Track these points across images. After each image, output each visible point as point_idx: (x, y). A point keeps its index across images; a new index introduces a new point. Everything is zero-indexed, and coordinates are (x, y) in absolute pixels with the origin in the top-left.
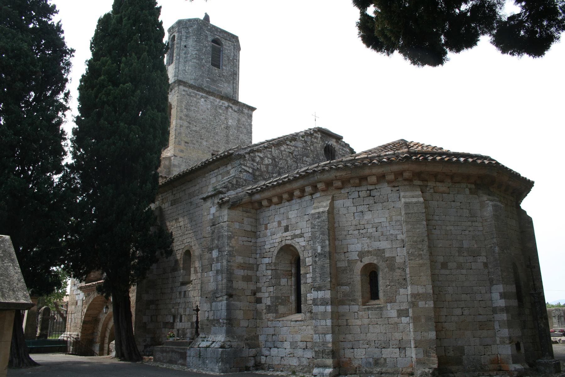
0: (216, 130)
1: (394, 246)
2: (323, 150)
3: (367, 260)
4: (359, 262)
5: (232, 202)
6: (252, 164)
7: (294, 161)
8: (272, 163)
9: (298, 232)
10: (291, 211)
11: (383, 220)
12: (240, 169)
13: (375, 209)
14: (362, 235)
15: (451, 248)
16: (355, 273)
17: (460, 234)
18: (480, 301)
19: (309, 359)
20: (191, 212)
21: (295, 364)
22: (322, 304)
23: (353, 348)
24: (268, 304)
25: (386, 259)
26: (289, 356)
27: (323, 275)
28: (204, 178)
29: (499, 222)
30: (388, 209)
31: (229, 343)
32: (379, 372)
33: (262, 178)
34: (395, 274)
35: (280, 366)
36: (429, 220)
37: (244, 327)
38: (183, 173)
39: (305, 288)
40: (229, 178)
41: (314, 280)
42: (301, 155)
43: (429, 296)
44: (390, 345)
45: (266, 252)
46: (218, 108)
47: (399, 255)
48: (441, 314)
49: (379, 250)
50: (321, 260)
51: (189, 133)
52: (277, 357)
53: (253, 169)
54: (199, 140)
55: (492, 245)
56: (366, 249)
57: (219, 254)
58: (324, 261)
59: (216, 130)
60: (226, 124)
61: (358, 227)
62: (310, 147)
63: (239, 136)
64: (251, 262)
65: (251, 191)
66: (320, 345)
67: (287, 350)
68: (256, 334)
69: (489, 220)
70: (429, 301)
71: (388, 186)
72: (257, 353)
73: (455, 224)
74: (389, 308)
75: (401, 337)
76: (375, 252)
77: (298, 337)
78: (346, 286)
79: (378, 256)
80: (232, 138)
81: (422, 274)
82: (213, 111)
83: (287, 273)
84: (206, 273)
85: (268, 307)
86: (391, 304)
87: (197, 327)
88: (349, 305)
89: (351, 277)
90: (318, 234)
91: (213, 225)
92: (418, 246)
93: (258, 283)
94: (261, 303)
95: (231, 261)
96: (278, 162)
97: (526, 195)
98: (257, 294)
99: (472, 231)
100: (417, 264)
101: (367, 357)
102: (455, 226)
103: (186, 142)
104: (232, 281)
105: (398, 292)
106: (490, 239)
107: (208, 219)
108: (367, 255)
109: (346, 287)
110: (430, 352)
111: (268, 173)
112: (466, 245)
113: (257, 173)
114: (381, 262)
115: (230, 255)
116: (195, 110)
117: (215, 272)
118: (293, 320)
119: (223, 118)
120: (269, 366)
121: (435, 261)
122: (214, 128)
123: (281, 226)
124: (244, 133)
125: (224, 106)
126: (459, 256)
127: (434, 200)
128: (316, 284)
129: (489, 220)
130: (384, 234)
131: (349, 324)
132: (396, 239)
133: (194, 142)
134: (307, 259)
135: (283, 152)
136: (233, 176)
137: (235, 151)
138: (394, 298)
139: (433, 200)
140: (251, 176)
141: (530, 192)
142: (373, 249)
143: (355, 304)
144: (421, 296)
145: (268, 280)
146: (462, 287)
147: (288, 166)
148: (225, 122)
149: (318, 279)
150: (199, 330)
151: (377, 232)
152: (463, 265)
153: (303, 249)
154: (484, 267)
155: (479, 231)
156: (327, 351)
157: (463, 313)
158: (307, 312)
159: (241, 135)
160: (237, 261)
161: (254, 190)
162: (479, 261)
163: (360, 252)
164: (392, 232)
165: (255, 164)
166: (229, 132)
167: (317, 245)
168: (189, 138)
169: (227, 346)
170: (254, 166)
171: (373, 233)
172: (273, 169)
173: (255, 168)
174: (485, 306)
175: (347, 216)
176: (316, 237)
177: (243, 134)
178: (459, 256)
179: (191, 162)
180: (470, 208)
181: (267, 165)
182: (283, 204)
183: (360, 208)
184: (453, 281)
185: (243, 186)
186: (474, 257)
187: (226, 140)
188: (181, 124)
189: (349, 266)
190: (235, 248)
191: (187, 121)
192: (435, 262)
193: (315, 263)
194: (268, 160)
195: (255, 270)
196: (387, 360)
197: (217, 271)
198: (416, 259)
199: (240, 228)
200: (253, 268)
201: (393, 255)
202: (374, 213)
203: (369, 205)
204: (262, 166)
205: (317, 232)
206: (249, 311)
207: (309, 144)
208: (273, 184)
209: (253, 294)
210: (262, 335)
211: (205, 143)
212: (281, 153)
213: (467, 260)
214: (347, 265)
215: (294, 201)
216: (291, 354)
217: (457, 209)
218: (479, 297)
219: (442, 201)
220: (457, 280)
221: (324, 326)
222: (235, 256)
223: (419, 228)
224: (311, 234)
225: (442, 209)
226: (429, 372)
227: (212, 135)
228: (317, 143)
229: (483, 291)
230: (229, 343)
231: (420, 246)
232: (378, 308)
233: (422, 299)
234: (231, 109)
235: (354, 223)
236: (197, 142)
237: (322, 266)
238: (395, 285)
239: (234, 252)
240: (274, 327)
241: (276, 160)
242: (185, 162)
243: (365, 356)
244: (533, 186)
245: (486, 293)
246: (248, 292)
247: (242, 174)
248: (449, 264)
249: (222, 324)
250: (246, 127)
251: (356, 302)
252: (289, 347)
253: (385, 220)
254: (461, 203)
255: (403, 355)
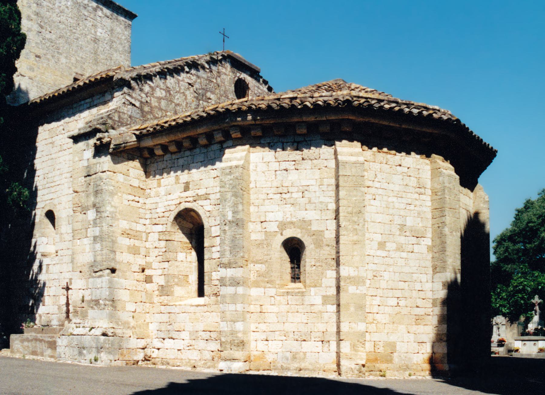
0: (80, 43)
1: (323, 218)
2: (233, 85)
3: (289, 233)
4: (279, 235)
5: (115, 145)
6: (139, 95)
7: (195, 97)
8: (166, 96)
9: (201, 192)
10: (193, 163)
11: (313, 182)
12: (123, 101)
13: (302, 167)
14: (285, 201)
15: (391, 224)
16: (273, 249)
17: (404, 208)
18: (419, 291)
19: (213, 352)
20: (53, 156)
21: (195, 358)
22: (231, 285)
23: (268, 339)
24: (160, 284)
25: (312, 233)
26: (188, 348)
27: (234, 249)
28: (71, 110)
29: (451, 196)
30: (319, 169)
31: (112, 330)
32: (297, 368)
33: (152, 116)
34: (322, 252)
35: (176, 360)
36: (368, 187)
37: (130, 311)
38: (41, 100)
39: (209, 264)
40: (108, 112)
41: (222, 254)
42: (203, 89)
43: (361, 280)
44: (312, 337)
45: (159, 217)
46: (82, 7)
47: (329, 229)
48: (373, 304)
49: (305, 221)
50: (232, 229)
51: (41, 42)
52: (173, 350)
53: (141, 102)
54: (56, 54)
55: (440, 225)
56: (288, 220)
57: (97, 215)
58: (235, 230)
59: (80, 43)
60: (93, 34)
61: (280, 190)
62: (216, 79)
63: (112, 55)
64: (138, 229)
65: (139, 132)
66: (228, 335)
67: (185, 341)
68: (145, 321)
69: (439, 194)
70: (361, 286)
71: (320, 139)
72: (148, 344)
73: (398, 196)
74: (312, 293)
75: (325, 328)
76: (300, 224)
77: (200, 326)
78: (261, 263)
79: (303, 229)
80: (102, 56)
81: (355, 253)
82: (75, 11)
83: (185, 245)
84: (78, 240)
85: (160, 288)
86: (316, 288)
87: (68, 312)
88: (265, 288)
89: (269, 253)
90: (229, 195)
91: (89, 176)
92: (354, 219)
93: (147, 257)
94: (151, 282)
95: (114, 225)
96: (174, 97)
97: (486, 169)
98: (146, 270)
99: (418, 206)
100: (350, 241)
101: (284, 350)
102: (399, 198)
103: (37, 56)
104: (115, 252)
105: (324, 275)
106: (439, 217)
107: (81, 167)
108: (289, 226)
109: (261, 265)
110: (358, 346)
111: (161, 109)
112: (409, 222)
113: (146, 109)
114: (306, 236)
115: (113, 217)
116: (48, 6)
117: (92, 239)
118: (193, 304)
119: (89, 24)
120: (162, 361)
121: (371, 239)
122: (77, 39)
123: (179, 183)
124: (119, 51)
125: (92, 6)
126: (400, 235)
127: (376, 161)
128: (225, 260)
129: (439, 194)
130: (312, 202)
131: (263, 311)
132: (326, 208)
133: (48, 56)
134: (213, 229)
135: (181, 83)
136: (114, 109)
137: (116, 73)
138: (320, 281)
139: (375, 162)
140: (138, 111)
141: (492, 164)
142: (297, 219)
143: (271, 286)
144: (352, 280)
145: (161, 254)
146: (400, 273)
147: (187, 103)
148: (93, 31)
149: (227, 253)
150: (71, 315)
151: (303, 197)
152: (404, 246)
153: (208, 214)
154: (428, 251)
155: (426, 206)
156: (236, 341)
157: (398, 303)
158: (211, 295)
159: (115, 55)
160: (121, 226)
161: (145, 131)
162: (423, 243)
163: (281, 223)
164: (322, 199)
165: (144, 95)
166: (98, 47)
167: (227, 210)
168: (41, 50)
169: (110, 334)
170: (142, 98)
171: (298, 199)
172: (168, 105)
173: (143, 100)
174: (424, 298)
175: (266, 174)
176: (227, 199)
177: (118, 53)
178: (400, 235)
179: (45, 87)
180: (418, 176)
181: (159, 99)
182: (182, 153)
183: (284, 165)
184: (391, 265)
185: (127, 125)
186: (417, 237)
187: (93, 58)
188: (29, 26)
189: (267, 240)
190: (118, 209)
191: (38, 23)
192: (371, 241)
193: (224, 232)
194: (161, 92)
195: (144, 239)
196: (308, 354)
197: (95, 238)
198: (349, 234)
199: (125, 182)
200: (141, 237)
201: (321, 229)
202: (301, 172)
203: (295, 161)
204: (152, 99)
205: (227, 193)
206: (136, 292)
207: (215, 75)
208: (170, 125)
209: (141, 271)
210: (153, 323)
211: (63, 60)
212: (179, 84)
213: (408, 241)
214: (263, 238)
215: (197, 150)
216: (191, 346)
217: (404, 176)
218: (418, 286)
219: (386, 164)
220: (395, 264)
221: (233, 312)
222: (118, 219)
223: (356, 196)
224: (221, 195)
225: (385, 174)
226: (355, 368)
227: (75, 48)
228: (225, 74)
229: (424, 280)
230: (112, 330)
231: (355, 219)
232: (299, 292)
233: (353, 283)
234: (101, 11)
235: (275, 184)
236: (53, 56)
237: (233, 237)
238: (322, 266)
239: (117, 215)
240: (169, 313)
241: (172, 92)
242: (37, 86)
243: (281, 349)
244: (495, 156)
245: (427, 282)
246: (137, 268)
247: (127, 108)
248: (388, 244)
249: (103, 306)
250: (122, 42)
251: (272, 284)
252: (188, 338)
253: (315, 183)
254: (408, 168)
255: (326, 349)
